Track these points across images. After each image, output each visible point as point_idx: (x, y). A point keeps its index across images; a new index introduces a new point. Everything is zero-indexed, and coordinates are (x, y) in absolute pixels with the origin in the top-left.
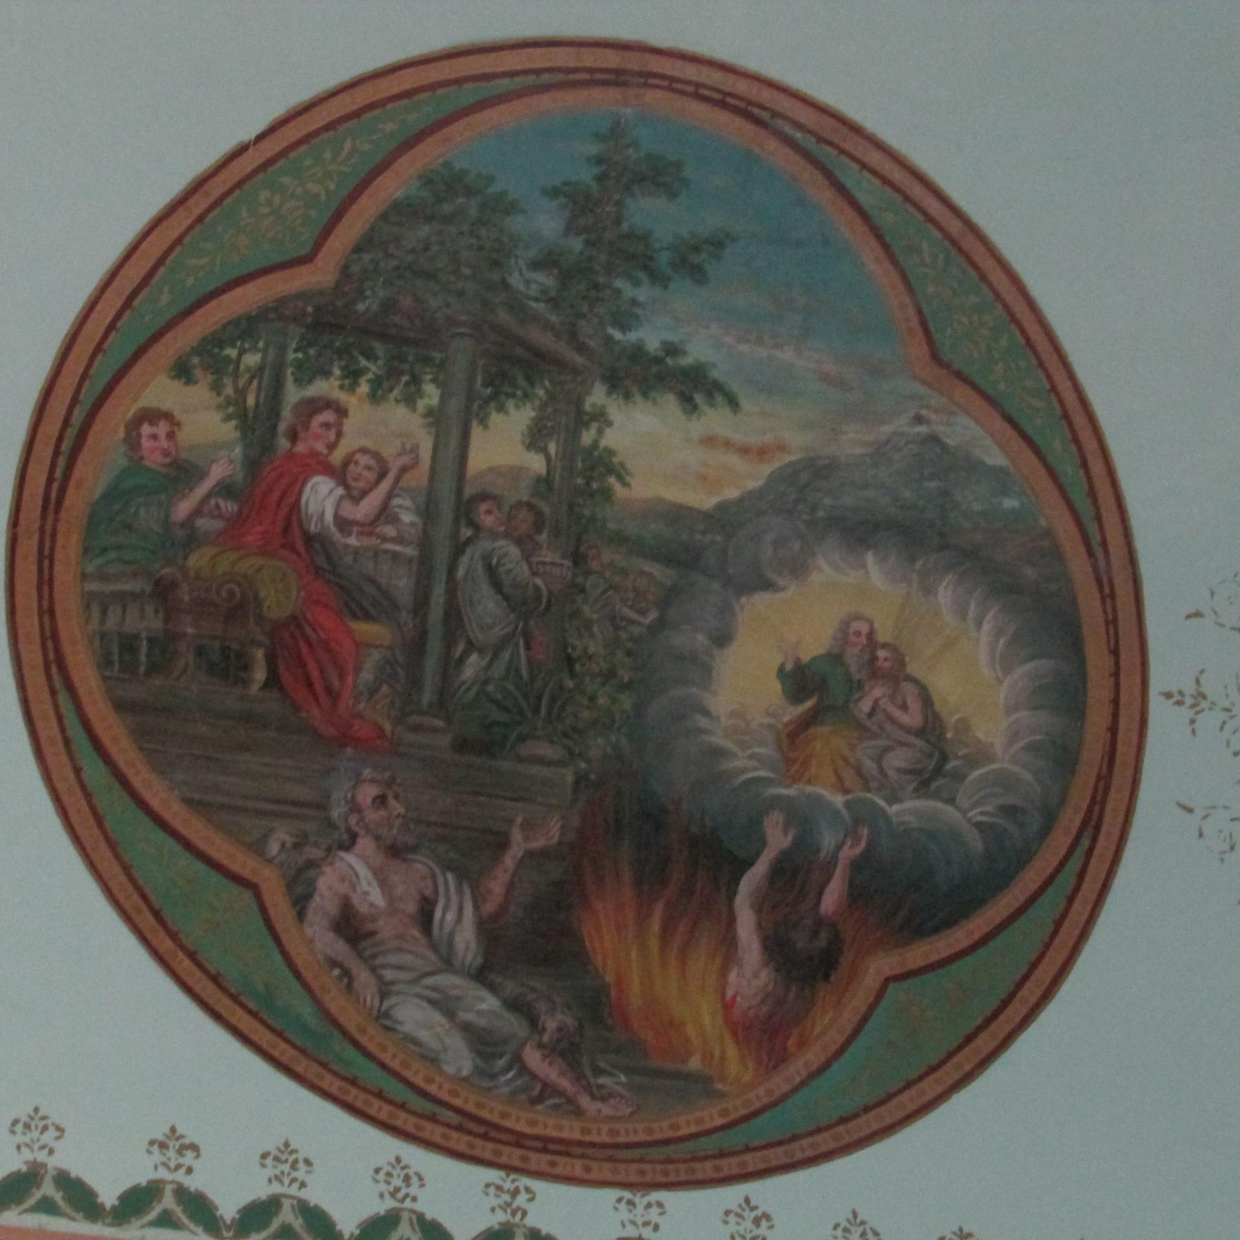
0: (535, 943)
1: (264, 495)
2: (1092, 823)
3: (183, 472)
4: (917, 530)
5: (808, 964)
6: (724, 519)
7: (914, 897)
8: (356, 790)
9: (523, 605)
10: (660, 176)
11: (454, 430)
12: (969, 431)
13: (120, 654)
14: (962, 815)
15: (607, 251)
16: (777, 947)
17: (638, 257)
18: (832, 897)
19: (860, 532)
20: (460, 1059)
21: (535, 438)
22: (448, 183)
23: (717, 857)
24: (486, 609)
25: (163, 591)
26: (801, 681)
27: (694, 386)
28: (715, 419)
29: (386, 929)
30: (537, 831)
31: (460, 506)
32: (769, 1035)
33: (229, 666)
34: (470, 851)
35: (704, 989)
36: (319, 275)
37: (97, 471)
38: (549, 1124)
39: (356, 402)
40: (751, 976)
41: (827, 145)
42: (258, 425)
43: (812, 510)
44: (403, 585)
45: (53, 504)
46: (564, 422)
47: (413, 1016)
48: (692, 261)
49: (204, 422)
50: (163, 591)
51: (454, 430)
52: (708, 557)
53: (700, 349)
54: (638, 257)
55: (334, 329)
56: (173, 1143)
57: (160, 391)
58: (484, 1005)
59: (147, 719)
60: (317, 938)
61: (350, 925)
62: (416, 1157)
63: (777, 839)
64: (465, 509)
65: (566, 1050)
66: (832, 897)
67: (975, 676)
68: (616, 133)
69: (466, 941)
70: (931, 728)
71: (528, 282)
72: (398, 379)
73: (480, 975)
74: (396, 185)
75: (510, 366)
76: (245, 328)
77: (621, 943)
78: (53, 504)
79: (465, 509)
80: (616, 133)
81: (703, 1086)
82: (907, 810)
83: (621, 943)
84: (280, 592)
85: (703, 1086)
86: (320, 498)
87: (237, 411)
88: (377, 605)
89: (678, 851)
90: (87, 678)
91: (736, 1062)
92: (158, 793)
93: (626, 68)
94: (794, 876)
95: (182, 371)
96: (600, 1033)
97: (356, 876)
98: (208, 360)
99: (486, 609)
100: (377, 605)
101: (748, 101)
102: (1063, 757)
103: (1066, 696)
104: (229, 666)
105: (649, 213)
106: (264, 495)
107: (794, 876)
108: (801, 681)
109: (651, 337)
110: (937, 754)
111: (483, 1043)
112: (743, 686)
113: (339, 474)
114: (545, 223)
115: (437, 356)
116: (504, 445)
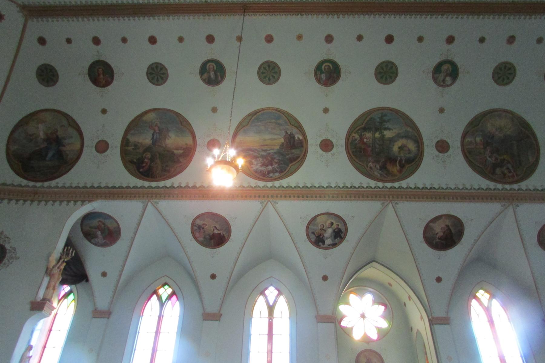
0: (383, 168)
1: (361, 139)
2: (421, 155)
3: (356, 140)
4: (407, 137)
5: (402, 166)
6: (393, 138)
7: (409, 161)
8: (370, 159)
9: (379, 145)
10: (386, 115)
11: (373, 134)
12: (409, 129)
13: (353, 152)
14: (412, 155)
15: (382, 121)
16: (400, 166)
17: (385, 121)
18: (403, 162)
19: (403, 137)
20: (379, 176)
21: (379, 134)
22: (371, 118)
23: (395, 161)
24: (377, 146)
25: (355, 148)
26: (399, 148)
27: (389, 129)
28: (391, 131)
29: (373, 168)
30: (382, 160)
31: (374, 139)
32: (400, 171)
33: (361, 152)
34: (378, 162)
35: (395, 169)
36: (363, 126)
37: (350, 140)
38: (386, 179)
39: (367, 133)
40: (398, 168)
41: (397, 112)
42: (361, 136)
43: (399, 136)
44: (371, 145)
45: (348, 142)
46: (381, 133)
47: (376, 173)
48: (388, 121)
49: (357, 136)
50: (355, 148)
51: (373, 134)
52: (392, 140)
53: (390, 126)
54: (385, 121)
55: (365, 129)
56: (329, 183)
57: (354, 135)
58: (380, 172)
59: (355, 156)
60: (368, 169)
61: (371, 168)
62: (497, 184)
63: (399, 159)
64: (375, 139)
65: (387, 175)
66: (403, 162)
67: (411, 146)
68: (382, 113)
69: (379, 168)
70: (409, 150)
71: (378, 124)
72: (369, 132)
73: (380, 170)
74: (367, 119)
75: (377, 130)
76: (359, 130)
77: (389, 167)
78: (348, 142)
79: (375, 139)
80: (382, 113)
81: (395, 176)
82: (408, 155)
83: (389, 167)
84: (363, 147)
85: (395, 176)
86: (365, 140)
87: (359, 135)
88: (369, 147)
89: (392, 160)
90: (351, 154)
91: (398, 174)
92: (357, 161)
93: (382, 109)
94: (400, 161)
95: (355, 133)
96: (389, 173)
97: (371, 164)
98: (357, 132)
99: (377, 146)
100: (369, 147)
101: (391, 110)
102: (418, 150)
103: (418, 147)
104: (361, 152)
105: (385, 118)
106: (361, 139)
107: (400, 161)
108: (399, 148)
109: (386, 126)
110: (410, 151)
111: (381, 174)
112: (395, 149)
113: (366, 138)
114: (378, 120)
115: (391, 199)
116: (377, 135)
